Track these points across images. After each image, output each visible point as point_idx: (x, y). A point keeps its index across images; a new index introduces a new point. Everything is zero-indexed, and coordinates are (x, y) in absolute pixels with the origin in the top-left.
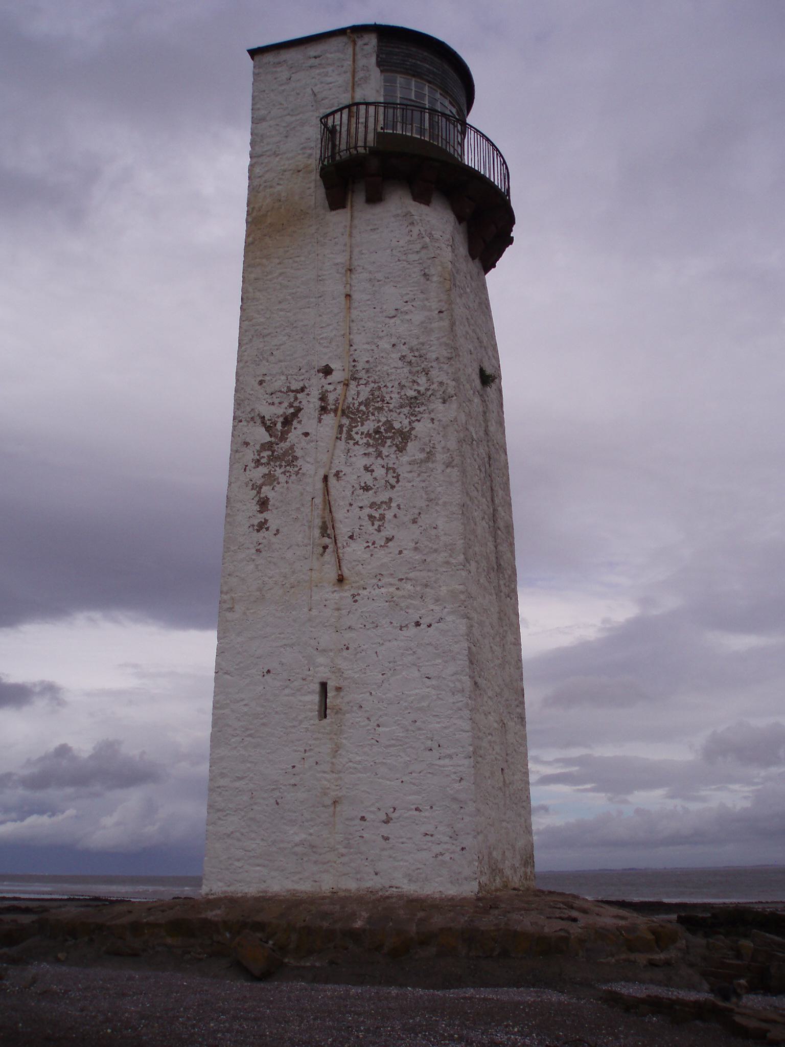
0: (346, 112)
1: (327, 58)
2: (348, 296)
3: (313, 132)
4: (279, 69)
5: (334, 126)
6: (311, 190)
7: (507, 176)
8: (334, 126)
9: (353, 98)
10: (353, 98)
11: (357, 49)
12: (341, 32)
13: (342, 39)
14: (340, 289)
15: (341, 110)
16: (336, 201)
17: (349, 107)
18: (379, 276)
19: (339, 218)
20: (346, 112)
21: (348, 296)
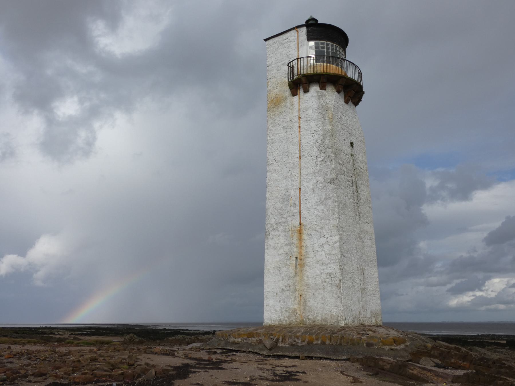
0: (296, 61)
1: (394, 358)
2: (300, 127)
3: (285, 69)
4: (268, 359)
5: (293, 66)
6: (287, 92)
7: (360, 74)
8: (293, 66)
9: (298, 55)
10: (298, 55)
11: (299, 34)
12: (293, 29)
13: (294, 31)
14: (298, 125)
15: (295, 60)
16: (294, 94)
17: (298, 59)
18: (309, 119)
19: (296, 98)
20: (296, 61)
21: (300, 127)
